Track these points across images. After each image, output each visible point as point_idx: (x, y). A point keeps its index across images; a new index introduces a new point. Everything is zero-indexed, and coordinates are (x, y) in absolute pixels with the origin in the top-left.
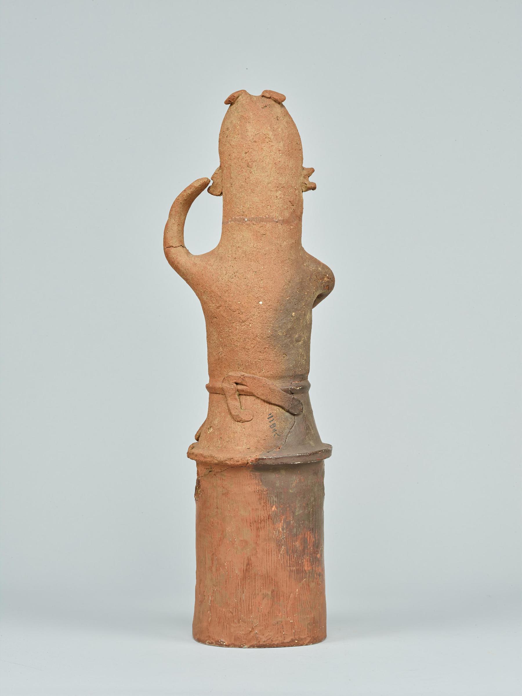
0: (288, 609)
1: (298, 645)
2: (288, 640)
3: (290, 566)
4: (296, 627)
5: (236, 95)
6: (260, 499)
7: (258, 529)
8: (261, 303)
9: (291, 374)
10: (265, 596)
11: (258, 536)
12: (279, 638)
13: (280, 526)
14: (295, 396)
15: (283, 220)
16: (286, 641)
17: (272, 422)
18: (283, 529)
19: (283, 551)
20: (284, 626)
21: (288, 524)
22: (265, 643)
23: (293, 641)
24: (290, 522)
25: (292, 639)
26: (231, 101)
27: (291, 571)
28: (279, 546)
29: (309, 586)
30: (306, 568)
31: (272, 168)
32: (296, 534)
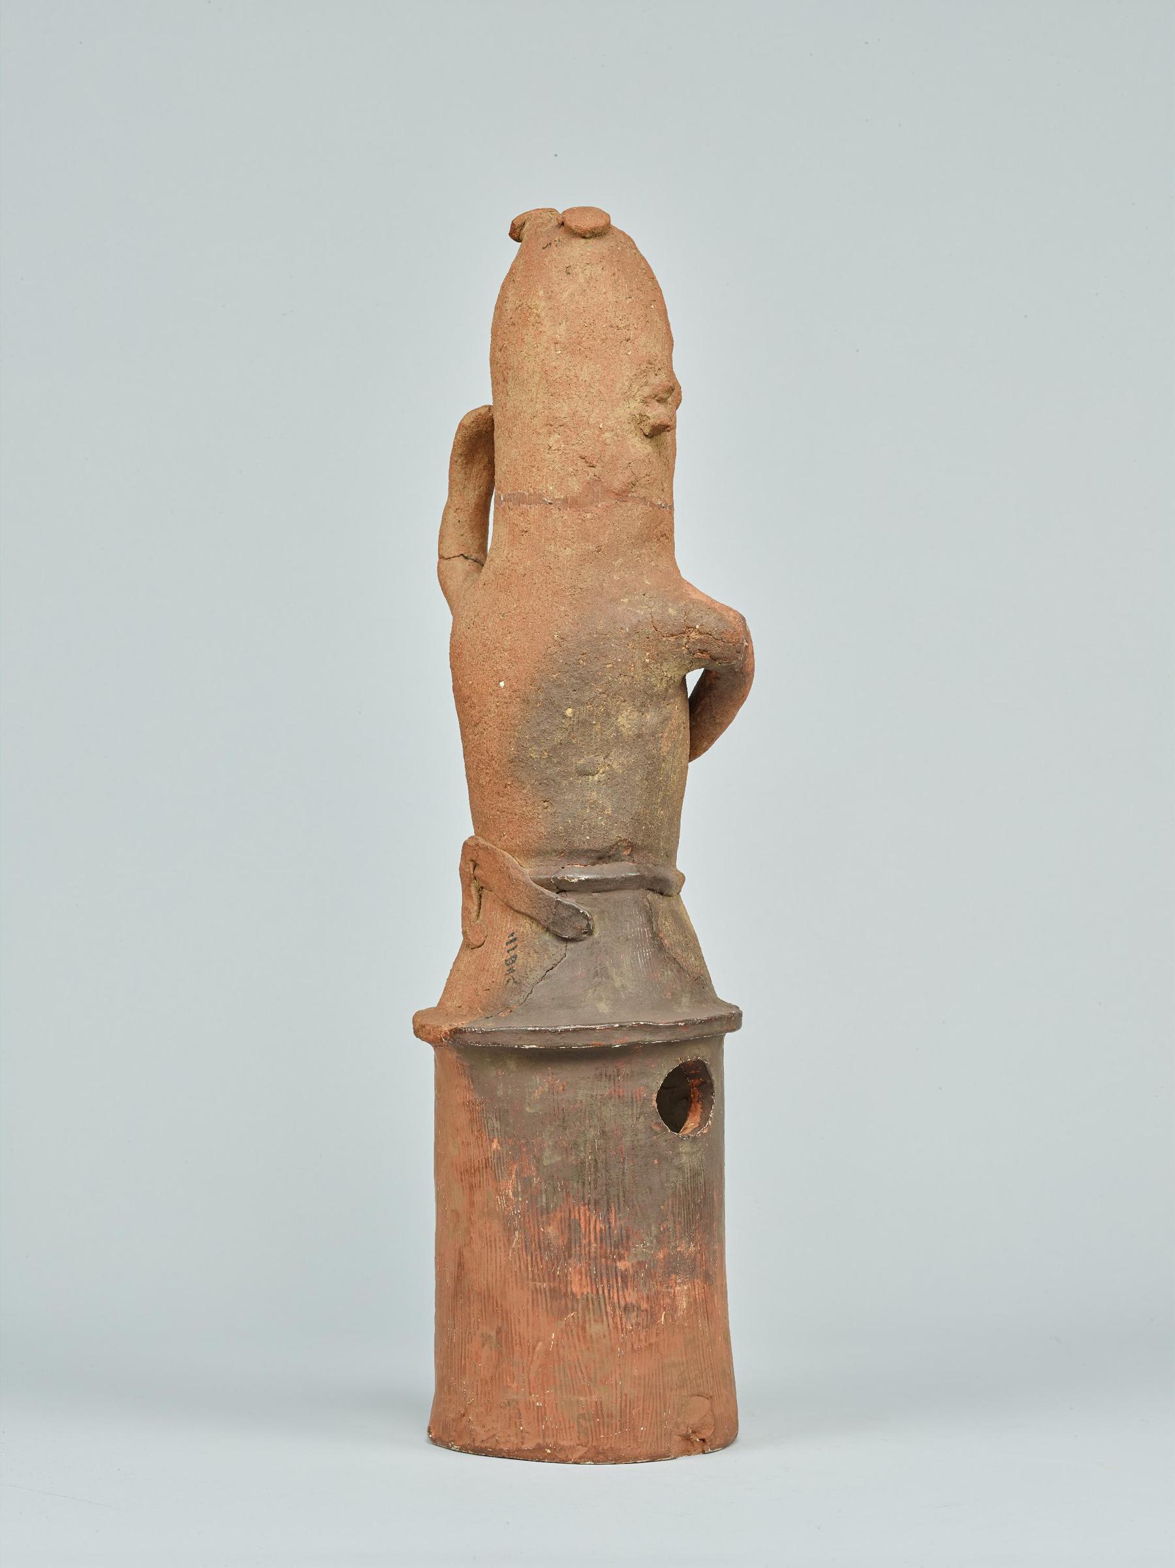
0: (532, 1375)
1: (553, 1459)
2: (529, 1445)
3: (534, 1280)
4: (549, 1418)
5: (518, 223)
6: (472, 1121)
7: (471, 1187)
8: (502, 684)
9: (559, 847)
10: (486, 1339)
11: (472, 1204)
12: (513, 1439)
13: (510, 1186)
14: (569, 900)
15: (565, 500)
16: (525, 1447)
17: (512, 953)
18: (515, 1194)
19: (518, 1243)
20: (523, 1412)
21: (527, 1183)
22: (483, 1446)
23: (540, 1448)
24: (530, 1179)
25: (539, 1444)
26: (516, 233)
27: (536, 1291)
28: (509, 1231)
29: (584, 1329)
30: (575, 1288)
31: (540, 382)
32: (547, 1209)
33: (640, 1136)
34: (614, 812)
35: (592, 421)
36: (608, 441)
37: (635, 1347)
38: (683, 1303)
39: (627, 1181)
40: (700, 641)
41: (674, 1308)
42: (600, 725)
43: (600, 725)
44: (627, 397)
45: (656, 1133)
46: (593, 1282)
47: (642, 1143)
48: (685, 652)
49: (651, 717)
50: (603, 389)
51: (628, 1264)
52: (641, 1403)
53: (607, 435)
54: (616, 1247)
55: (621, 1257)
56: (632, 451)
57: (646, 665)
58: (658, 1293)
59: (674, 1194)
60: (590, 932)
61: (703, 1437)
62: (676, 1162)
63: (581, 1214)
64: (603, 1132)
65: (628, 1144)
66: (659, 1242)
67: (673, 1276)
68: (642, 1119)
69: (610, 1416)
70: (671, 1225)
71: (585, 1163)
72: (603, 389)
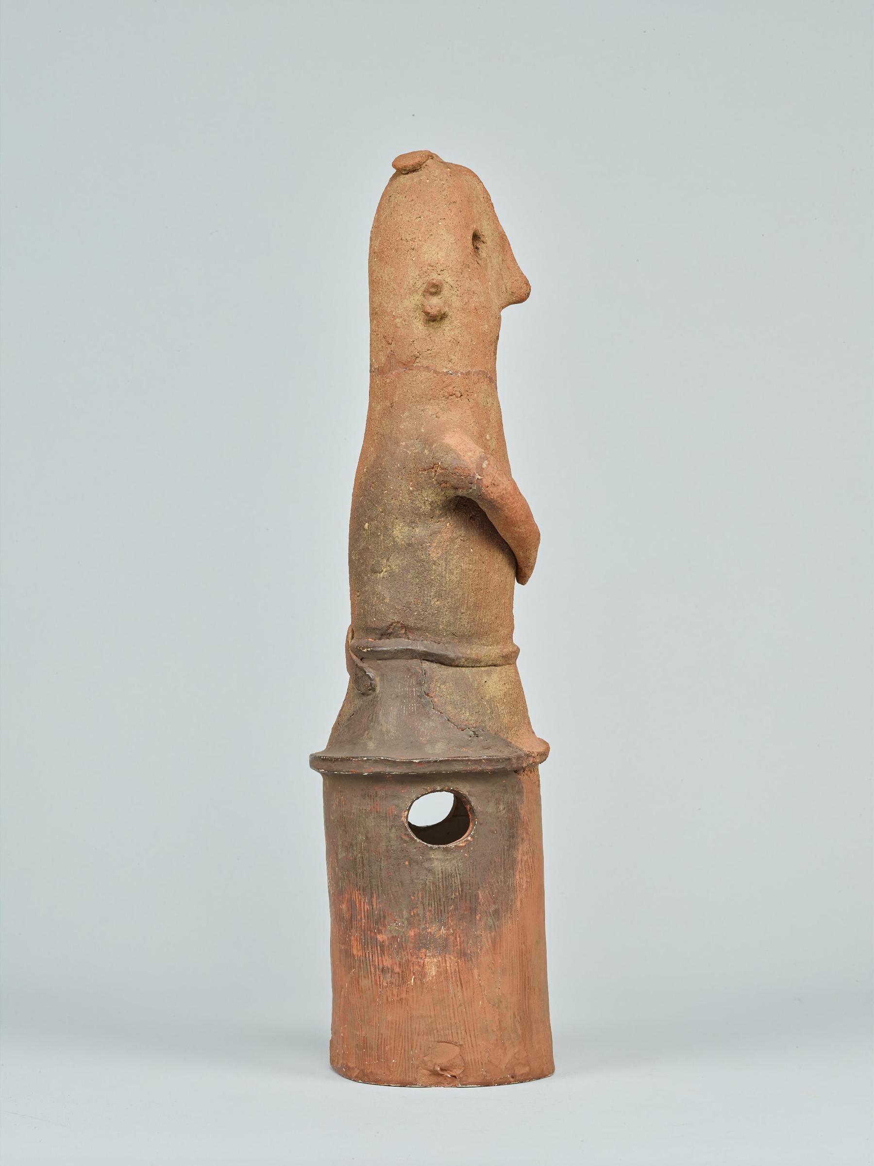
30: (355, 952)
33: (393, 843)
34: (390, 601)
35: (389, 310)
36: (398, 325)
37: (390, 1000)
38: (432, 971)
39: (383, 874)
40: (441, 474)
41: (423, 974)
42: (447, 530)
43: (447, 530)
44: (413, 291)
45: (406, 842)
46: (364, 949)
47: (394, 848)
48: (435, 483)
49: (419, 531)
50: (395, 286)
51: (385, 937)
52: (392, 1041)
53: (398, 320)
54: (377, 923)
55: (380, 932)
56: (416, 332)
57: (412, 492)
58: (408, 961)
59: (424, 889)
60: (374, 690)
61: (454, 1074)
62: (426, 865)
63: (357, 896)
64: (367, 838)
65: (384, 847)
66: (409, 923)
67: (424, 950)
68: (393, 830)
69: (371, 1048)
70: (421, 912)
71: (431, 863)
72: (395, 286)
